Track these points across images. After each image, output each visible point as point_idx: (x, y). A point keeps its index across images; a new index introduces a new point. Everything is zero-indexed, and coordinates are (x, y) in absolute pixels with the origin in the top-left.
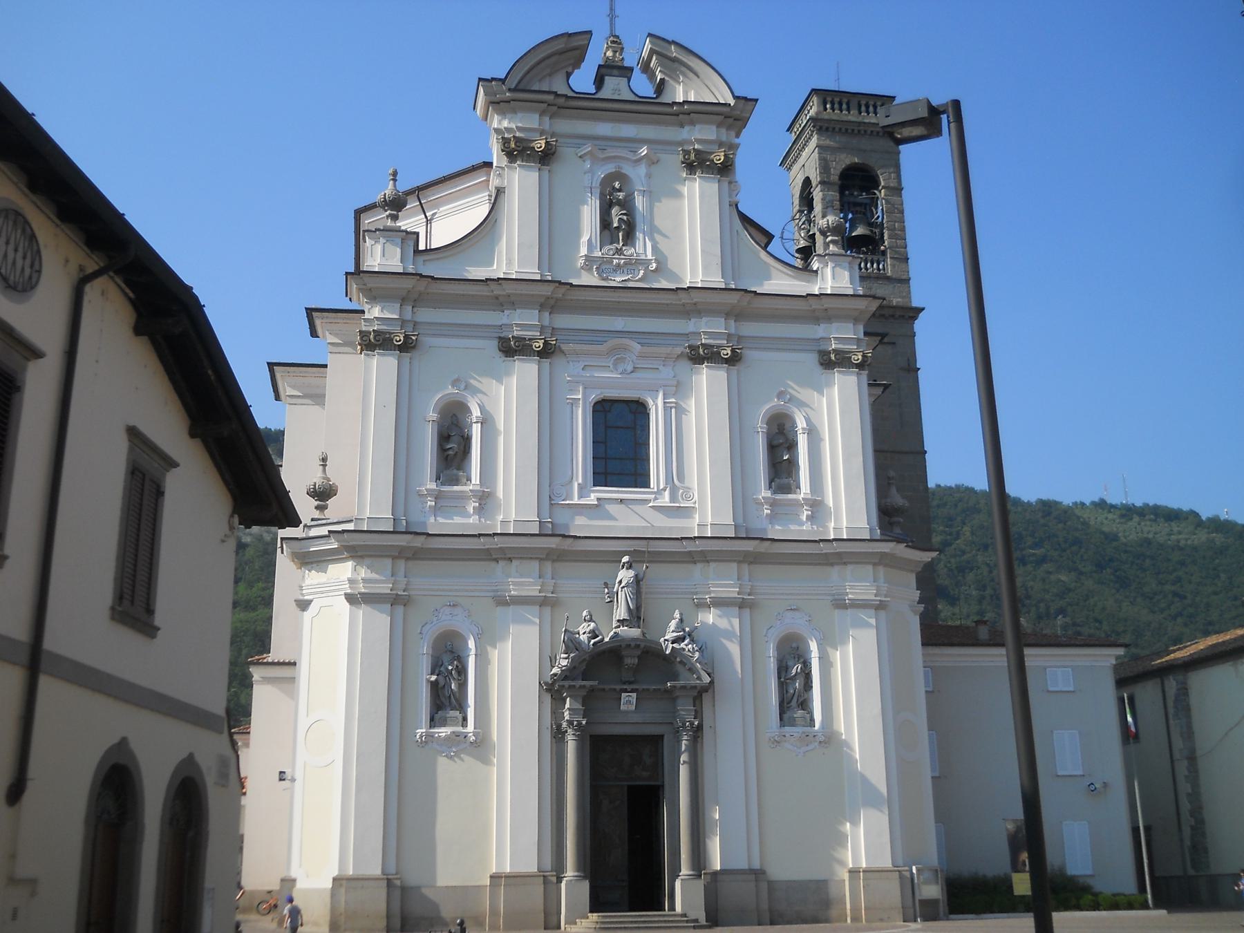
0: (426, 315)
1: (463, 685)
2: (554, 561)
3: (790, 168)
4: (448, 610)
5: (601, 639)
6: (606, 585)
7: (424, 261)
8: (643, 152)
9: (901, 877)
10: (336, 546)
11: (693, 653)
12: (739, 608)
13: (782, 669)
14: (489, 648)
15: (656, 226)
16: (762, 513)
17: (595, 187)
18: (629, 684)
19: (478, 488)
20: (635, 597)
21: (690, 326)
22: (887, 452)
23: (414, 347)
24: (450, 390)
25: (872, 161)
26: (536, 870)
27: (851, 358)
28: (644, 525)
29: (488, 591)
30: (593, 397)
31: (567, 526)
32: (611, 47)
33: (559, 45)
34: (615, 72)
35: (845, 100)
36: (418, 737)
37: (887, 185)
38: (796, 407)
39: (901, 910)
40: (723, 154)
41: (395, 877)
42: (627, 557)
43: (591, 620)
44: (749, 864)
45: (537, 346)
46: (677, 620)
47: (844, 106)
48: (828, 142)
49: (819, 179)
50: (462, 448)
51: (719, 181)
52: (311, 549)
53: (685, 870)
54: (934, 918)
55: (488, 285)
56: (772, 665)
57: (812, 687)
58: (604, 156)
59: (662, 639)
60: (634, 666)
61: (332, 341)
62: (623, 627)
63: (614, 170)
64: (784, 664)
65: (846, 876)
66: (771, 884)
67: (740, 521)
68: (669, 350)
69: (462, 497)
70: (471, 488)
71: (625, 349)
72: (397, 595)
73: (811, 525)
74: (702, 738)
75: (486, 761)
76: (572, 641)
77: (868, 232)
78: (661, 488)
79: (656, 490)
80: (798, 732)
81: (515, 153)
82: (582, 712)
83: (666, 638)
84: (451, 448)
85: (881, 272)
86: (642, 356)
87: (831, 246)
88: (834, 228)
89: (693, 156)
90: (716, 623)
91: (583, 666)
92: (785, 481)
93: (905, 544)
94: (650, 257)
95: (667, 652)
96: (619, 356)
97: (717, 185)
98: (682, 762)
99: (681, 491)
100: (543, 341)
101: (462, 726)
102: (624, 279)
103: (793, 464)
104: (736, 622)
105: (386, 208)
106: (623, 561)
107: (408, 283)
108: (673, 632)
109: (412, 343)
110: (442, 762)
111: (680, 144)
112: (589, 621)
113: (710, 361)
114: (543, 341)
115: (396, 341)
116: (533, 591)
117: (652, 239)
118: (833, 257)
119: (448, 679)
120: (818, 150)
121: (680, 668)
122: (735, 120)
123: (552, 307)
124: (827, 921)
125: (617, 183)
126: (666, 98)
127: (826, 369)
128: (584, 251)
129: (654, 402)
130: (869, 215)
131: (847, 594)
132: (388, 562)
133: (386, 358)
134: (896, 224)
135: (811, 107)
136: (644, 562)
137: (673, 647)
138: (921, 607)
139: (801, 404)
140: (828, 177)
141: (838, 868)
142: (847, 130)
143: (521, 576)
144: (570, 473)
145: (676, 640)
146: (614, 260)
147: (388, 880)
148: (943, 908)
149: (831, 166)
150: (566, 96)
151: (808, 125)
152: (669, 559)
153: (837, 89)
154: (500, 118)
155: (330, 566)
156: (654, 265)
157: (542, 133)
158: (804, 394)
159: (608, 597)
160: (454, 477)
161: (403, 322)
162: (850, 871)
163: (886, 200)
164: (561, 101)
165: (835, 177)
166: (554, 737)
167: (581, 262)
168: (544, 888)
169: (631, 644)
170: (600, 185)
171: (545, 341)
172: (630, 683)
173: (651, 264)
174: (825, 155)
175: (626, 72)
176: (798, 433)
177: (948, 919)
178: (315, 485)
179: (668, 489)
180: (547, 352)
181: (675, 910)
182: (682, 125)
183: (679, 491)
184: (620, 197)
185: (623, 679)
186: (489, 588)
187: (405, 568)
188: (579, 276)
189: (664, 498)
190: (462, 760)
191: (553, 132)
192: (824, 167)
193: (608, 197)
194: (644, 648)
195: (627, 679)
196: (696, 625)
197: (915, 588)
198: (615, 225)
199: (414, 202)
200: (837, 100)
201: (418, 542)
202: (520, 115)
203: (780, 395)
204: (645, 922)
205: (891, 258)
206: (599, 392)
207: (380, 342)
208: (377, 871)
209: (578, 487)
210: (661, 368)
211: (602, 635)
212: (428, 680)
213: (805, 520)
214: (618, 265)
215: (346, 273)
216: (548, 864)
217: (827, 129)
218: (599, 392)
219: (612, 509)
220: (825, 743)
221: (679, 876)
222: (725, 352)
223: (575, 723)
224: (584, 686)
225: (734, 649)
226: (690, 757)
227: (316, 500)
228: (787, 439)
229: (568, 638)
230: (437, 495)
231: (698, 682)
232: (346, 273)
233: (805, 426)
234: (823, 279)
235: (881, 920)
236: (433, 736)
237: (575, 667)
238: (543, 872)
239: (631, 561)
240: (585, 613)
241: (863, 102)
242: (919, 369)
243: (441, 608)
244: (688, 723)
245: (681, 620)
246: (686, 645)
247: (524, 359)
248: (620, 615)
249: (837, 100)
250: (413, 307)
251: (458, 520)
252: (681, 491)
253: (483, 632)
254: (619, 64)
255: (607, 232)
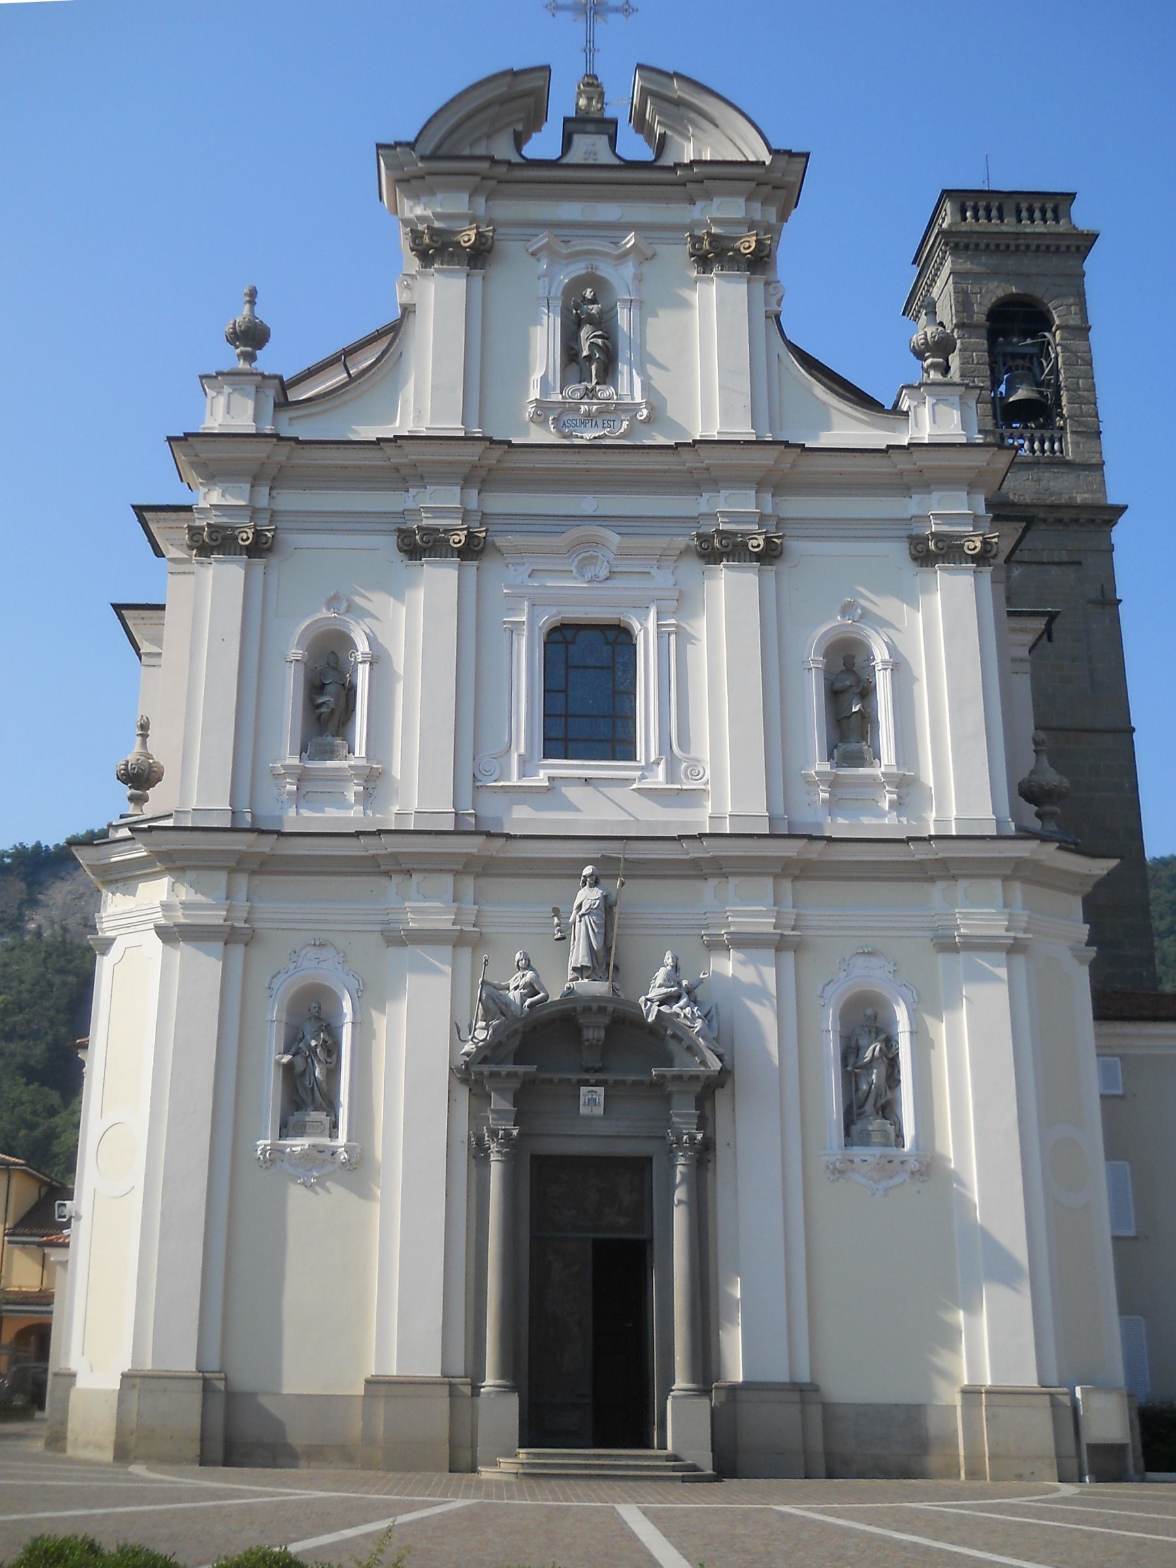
0: (290, 500)
1: (333, 1072)
2: (477, 876)
3: (917, 316)
4: (312, 953)
5: (543, 997)
6: (556, 912)
7: (290, 419)
8: (627, 243)
9: (1055, 1405)
10: (145, 854)
11: (693, 1020)
12: (777, 950)
13: (850, 1052)
14: (374, 1014)
15: (650, 355)
16: (816, 798)
17: (556, 298)
18: (594, 1073)
19: (363, 762)
20: (603, 931)
21: (704, 504)
22: (1069, 730)
23: (269, 550)
24: (325, 613)
25: (1038, 290)
26: (439, 1375)
27: (963, 545)
28: (623, 819)
29: (370, 922)
30: (546, 619)
31: (499, 821)
32: (584, 92)
33: (500, 89)
34: (590, 127)
35: (995, 204)
36: (259, 1152)
37: (1065, 324)
38: (870, 627)
39: (1055, 1461)
40: (755, 238)
41: (217, 1375)
42: (590, 867)
43: (528, 967)
44: (791, 1376)
45: (456, 541)
46: (669, 968)
47: (994, 213)
48: (968, 266)
49: (954, 322)
50: (342, 701)
51: (748, 282)
52: (113, 860)
53: (681, 1382)
54: (1119, 1477)
55: (381, 449)
56: (832, 1048)
57: (900, 1081)
58: (569, 251)
59: (643, 998)
60: (600, 1043)
61: (175, 556)
62: (582, 979)
63: (584, 272)
64: (853, 1044)
65: (958, 1400)
66: (827, 1407)
67: (779, 810)
68: (664, 542)
69: (338, 777)
70: (352, 763)
71: (597, 543)
72: (233, 927)
73: (898, 816)
74: (715, 1162)
75: (363, 1192)
76: (494, 1000)
77: (1034, 395)
78: (652, 761)
79: (643, 763)
80: (874, 1155)
81: (431, 252)
82: (513, 1116)
83: (648, 997)
84: (324, 703)
85: (1058, 454)
86: (622, 554)
87: (932, 373)
88: (935, 343)
89: (706, 245)
90: (737, 976)
91: (516, 1042)
92: (853, 746)
93: (1058, 844)
94: (638, 399)
95: (650, 1020)
96: (587, 554)
97: (746, 286)
98: (676, 1202)
99: (684, 765)
100: (465, 532)
101: (330, 1137)
102: (597, 435)
103: (867, 720)
104: (770, 973)
105: (237, 343)
106: (584, 874)
107: (261, 450)
108: (660, 986)
109: (265, 543)
110: (296, 1192)
111: (690, 227)
112: (525, 969)
113: (731, 559)
114: (465, 532)
115: (243, 540)
116: (444, 922)
117: (643, 372)
118: (933, 388)
119: (309, 1060)
120: (953, 278)
121: (673, 1046)
122: (774, 188)
123: (483, 481)
124: (922, 1475)
125: (589, 290)
126: (668, 160)
127: (921, 566)
128: (535, 393)
129: (641, 625)
130: (1037, 370)
131: (958, 927)
132: (222, 877)
133: (225, 567)
134: (1080, 381)
135: (944, 219)
136: (616, 876)
137: (659, 1010)
138: (1092, 952)
139: (881, 623)
140: (970, 317)
141: (942, 1387)
142: (998, 246)
143: (425, 898)
144: (507, 738)
145: (666, 1000)
146: (582, 406)
147: (205, 1380)
148: (1133, 1459)
149: (973, 301)
150: (509, 163)
151: (937, 244)
152: (662, 873)
153: (987, 189)
154: (411, 203)
155: (140, 885)
156: (645, 412)
157: (473, 219)
158: (884, 606)
159: (559, 931)
160: (328, 748)
161: (254, 511)
162: (965, 1392)
163: (1063, 347)
164: (502, 170)
165: (980, 317)
166: (474, 1157)
167: (531, 409)
168: (450, 1401)
169: (594, 1006)
170: (562, 295)
171: (469, 532)
172: (596, 1071)
173: (640, 410)
174: (965, 286)
175: (608, 127)
176: (876, 669)
177: (1143, 1480)
178: (126, 765)
179: (663, 761)
180: (472, 550)
181: (666, 1449)
182: (692, 200)
183: (681, 765)
184: (593, 311)
185: (584, 1064)
186: (371, 918)
187: (249, 889)
188: (527, 433)
189: (657, 777)
190: (328, 1191)
191: (491, 219)
192: (963, 302)
193: (574, 312)
194: (613, 1012)
195: (590, 1065)
196: (701, 976)
197: (1082, 920)
198: (585, 353)
199: (339, 374)
200: (982, 204)
201: (266, 845)
202: (440, 196)
203: (846, 609)
204: (601, 1467)
205: (1072, 432)
206: (554, 610)
207: (218, 543)
208: (188, 1365)
209: (519, 761)
210: (654, 571)
211: (545, 991)
212: (278, 1063)
213: (887, 809)
214: (588, 414)
215: (168, 438)
216: (458, 1367)
217: (967, 247)
218: (554, 610)
219: (573, 793)
220: (922, 1175)
221: (672, 1391)
222: (755, 543)
223: (501, 1133)
224: (514, 1075)
225: (766, 1017)
226: (690, 1192)
227: (130, 787)
228: (859, 680)
229: (487, 995)
230: (301, 775)
231: (702, 1069)
232: (168, 438)
233: (887, 657)
234: (916, 426)
235: (1019, 1477)
236: (283, 1152)
237: (500, 1044)
238: (449, 1377)
239: (597, 872)
240: (518, 956)
241: (1024, 206)
242: (1121, 601)
243: (301, 950)
244: (685, 1137)
245: (676, 968)
246: (682, 1008)
247: (436, 562)
248: (576, 960)
249: (982, 204)
250: (271, 489)
251: (331, 812)
252: (684, 765)
253: (364, 989)
254: (597, 116)
255: (574, 368)
